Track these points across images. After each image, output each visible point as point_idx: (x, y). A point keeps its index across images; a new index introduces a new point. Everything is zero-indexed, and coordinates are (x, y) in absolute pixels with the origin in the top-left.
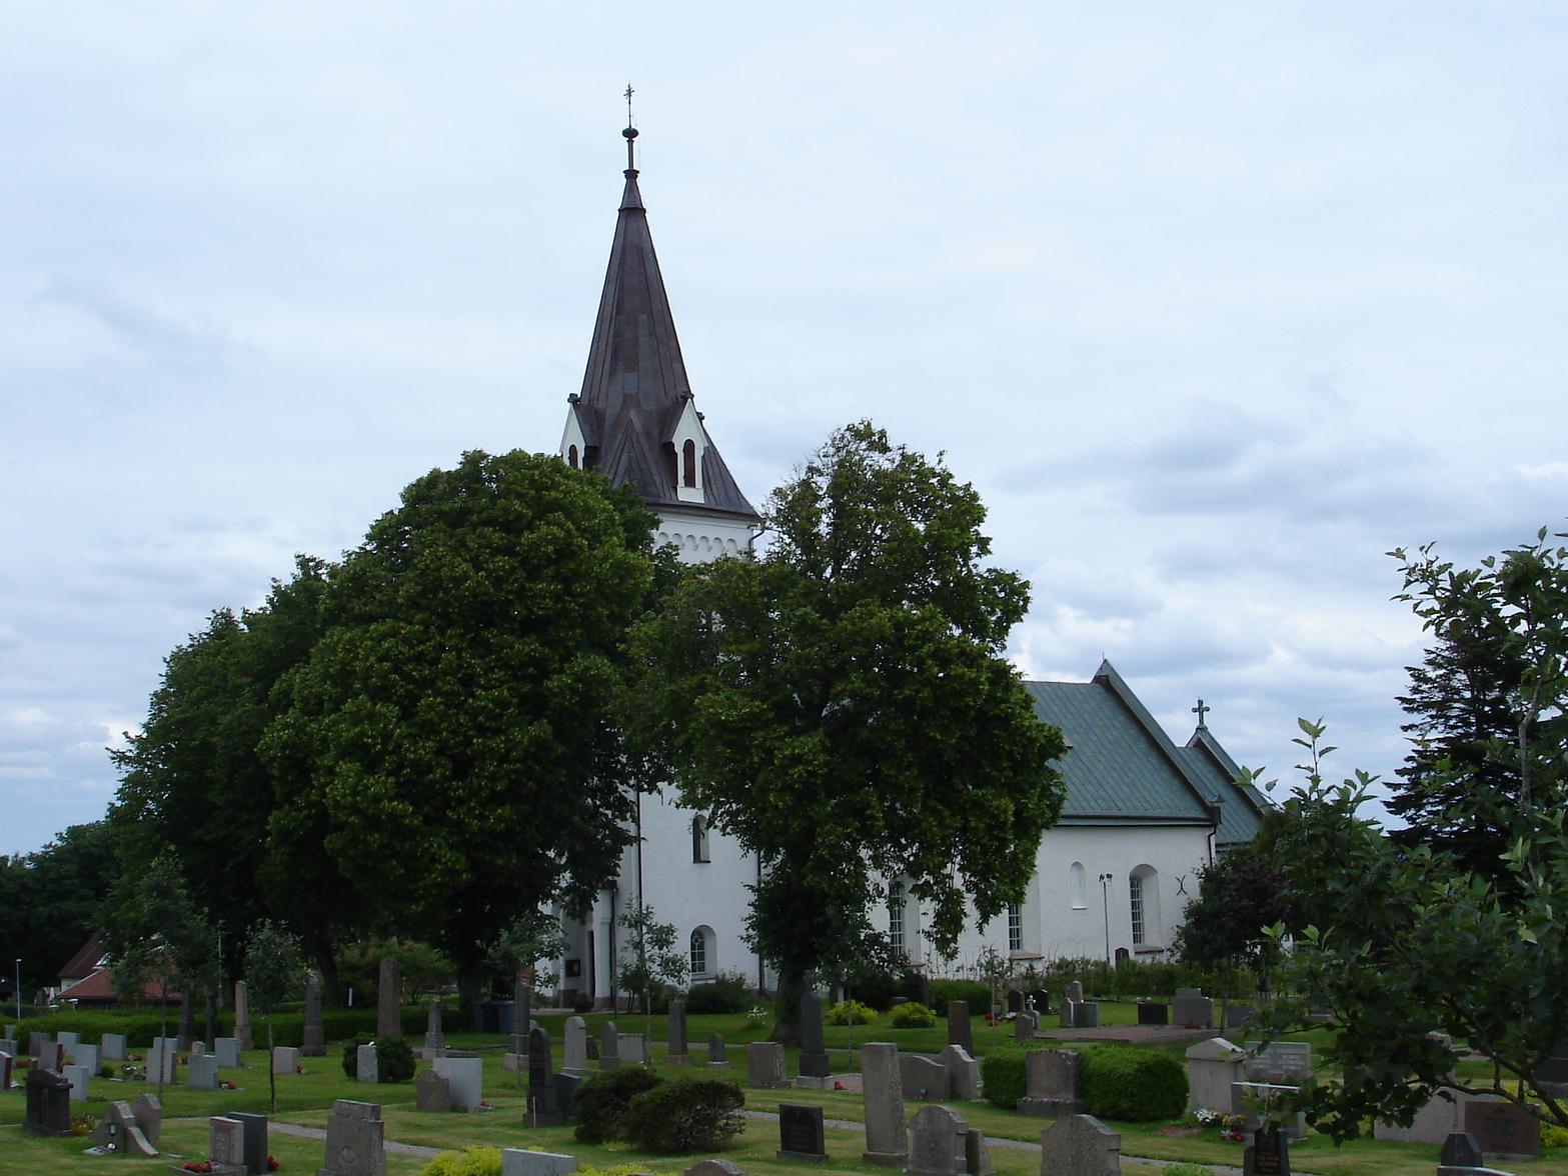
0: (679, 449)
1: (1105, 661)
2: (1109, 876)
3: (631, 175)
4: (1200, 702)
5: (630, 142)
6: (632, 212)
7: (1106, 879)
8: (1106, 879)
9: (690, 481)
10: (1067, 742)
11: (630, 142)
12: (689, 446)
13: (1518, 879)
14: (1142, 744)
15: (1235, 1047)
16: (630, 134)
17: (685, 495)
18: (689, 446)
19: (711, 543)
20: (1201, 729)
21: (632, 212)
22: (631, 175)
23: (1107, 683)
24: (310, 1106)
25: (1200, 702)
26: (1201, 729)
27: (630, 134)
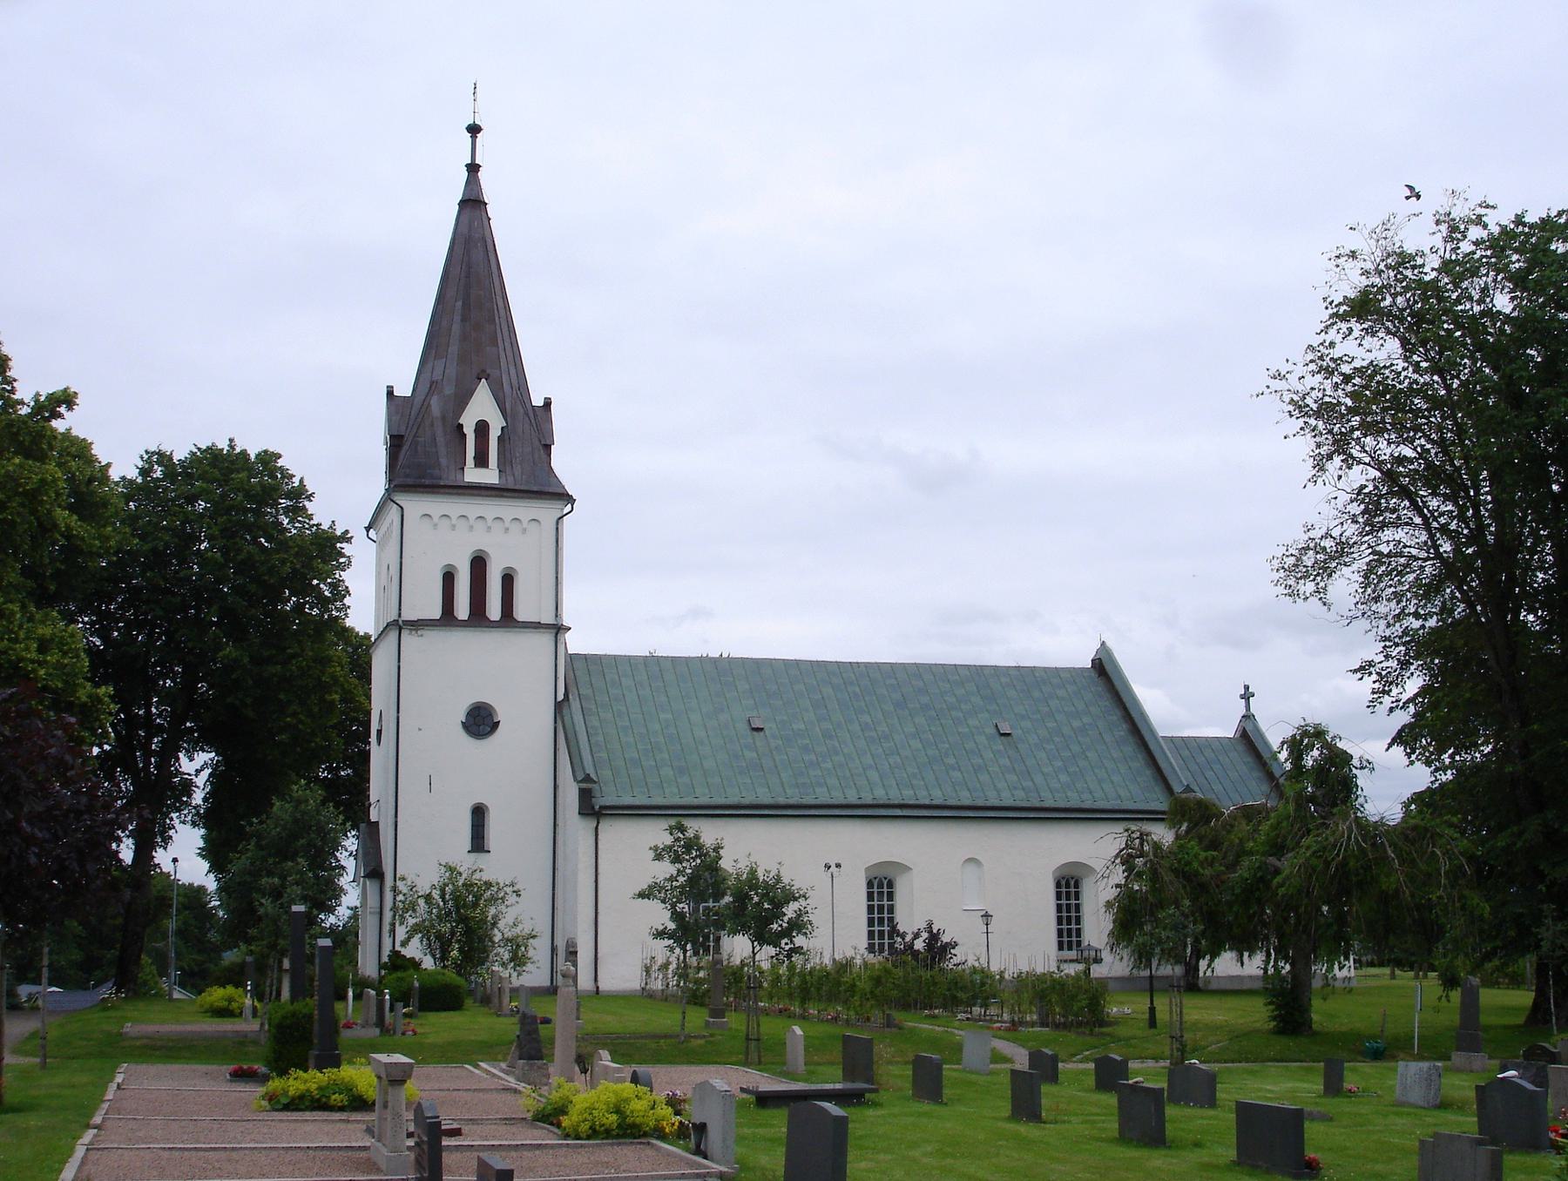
0: (469, 431)
1: (1103, 643)
2: (838, 866)
3: (473, 168)
4: (1247, 688)
5: (474, 137)
6: (473, 203)
7: (833, 868)
8: (833, 868)
9: (481, 461)
10: (1398, 750)
11: (474, 137)
12: (482, 428)
13: (351, 843)
14: (1122, 730)
15: (635, 1067)
16: (474, 130)
17: (473, 475)
18: (482, 428)
19: (507, 524)
20: (1248, 717)
21: (473, 203)
22: (473, 168)
23: (1103, 670)
24: (242, 1044)
25: (1247, 688)
26: (1248, 717)
27: (474, 130)
